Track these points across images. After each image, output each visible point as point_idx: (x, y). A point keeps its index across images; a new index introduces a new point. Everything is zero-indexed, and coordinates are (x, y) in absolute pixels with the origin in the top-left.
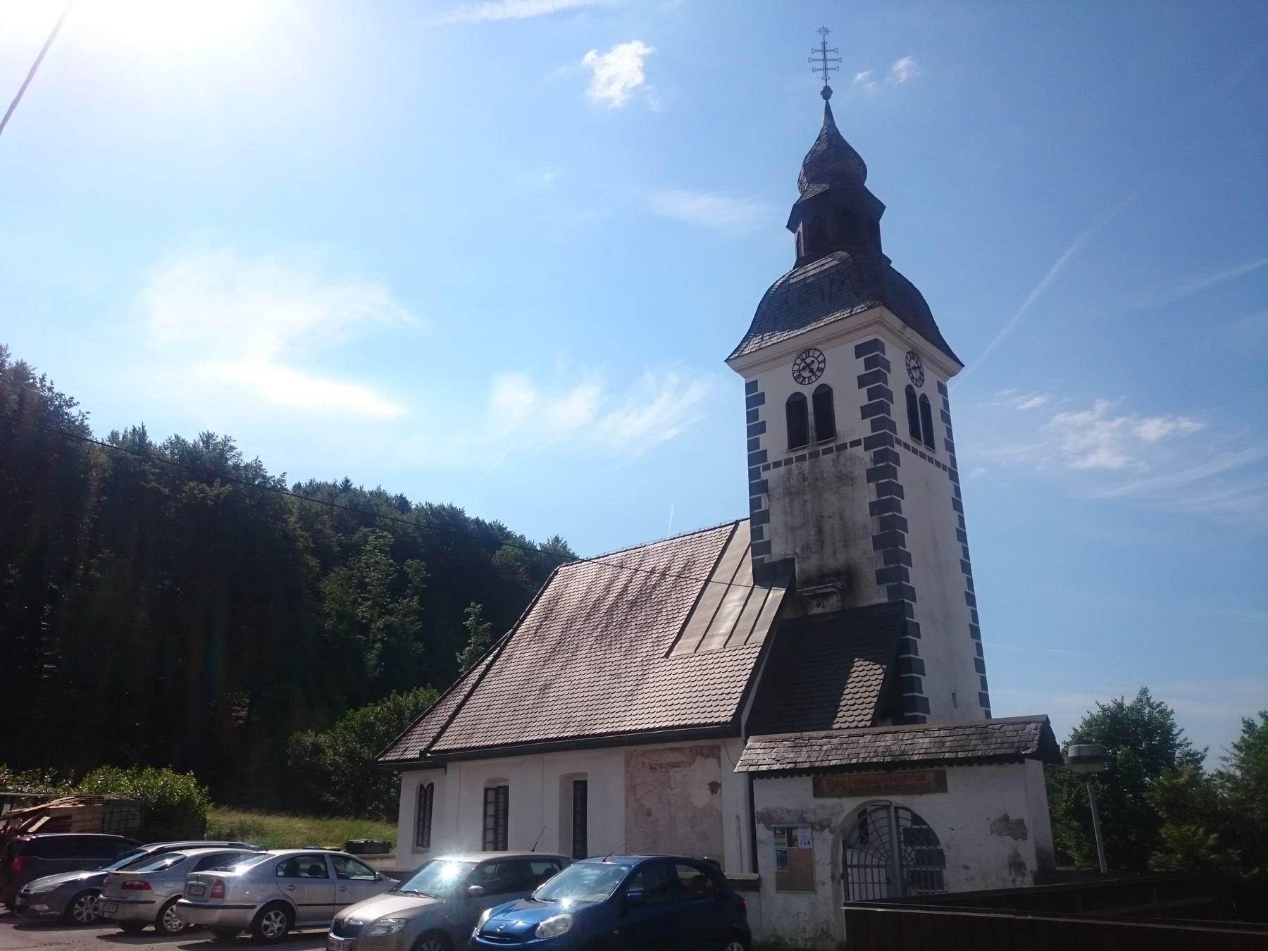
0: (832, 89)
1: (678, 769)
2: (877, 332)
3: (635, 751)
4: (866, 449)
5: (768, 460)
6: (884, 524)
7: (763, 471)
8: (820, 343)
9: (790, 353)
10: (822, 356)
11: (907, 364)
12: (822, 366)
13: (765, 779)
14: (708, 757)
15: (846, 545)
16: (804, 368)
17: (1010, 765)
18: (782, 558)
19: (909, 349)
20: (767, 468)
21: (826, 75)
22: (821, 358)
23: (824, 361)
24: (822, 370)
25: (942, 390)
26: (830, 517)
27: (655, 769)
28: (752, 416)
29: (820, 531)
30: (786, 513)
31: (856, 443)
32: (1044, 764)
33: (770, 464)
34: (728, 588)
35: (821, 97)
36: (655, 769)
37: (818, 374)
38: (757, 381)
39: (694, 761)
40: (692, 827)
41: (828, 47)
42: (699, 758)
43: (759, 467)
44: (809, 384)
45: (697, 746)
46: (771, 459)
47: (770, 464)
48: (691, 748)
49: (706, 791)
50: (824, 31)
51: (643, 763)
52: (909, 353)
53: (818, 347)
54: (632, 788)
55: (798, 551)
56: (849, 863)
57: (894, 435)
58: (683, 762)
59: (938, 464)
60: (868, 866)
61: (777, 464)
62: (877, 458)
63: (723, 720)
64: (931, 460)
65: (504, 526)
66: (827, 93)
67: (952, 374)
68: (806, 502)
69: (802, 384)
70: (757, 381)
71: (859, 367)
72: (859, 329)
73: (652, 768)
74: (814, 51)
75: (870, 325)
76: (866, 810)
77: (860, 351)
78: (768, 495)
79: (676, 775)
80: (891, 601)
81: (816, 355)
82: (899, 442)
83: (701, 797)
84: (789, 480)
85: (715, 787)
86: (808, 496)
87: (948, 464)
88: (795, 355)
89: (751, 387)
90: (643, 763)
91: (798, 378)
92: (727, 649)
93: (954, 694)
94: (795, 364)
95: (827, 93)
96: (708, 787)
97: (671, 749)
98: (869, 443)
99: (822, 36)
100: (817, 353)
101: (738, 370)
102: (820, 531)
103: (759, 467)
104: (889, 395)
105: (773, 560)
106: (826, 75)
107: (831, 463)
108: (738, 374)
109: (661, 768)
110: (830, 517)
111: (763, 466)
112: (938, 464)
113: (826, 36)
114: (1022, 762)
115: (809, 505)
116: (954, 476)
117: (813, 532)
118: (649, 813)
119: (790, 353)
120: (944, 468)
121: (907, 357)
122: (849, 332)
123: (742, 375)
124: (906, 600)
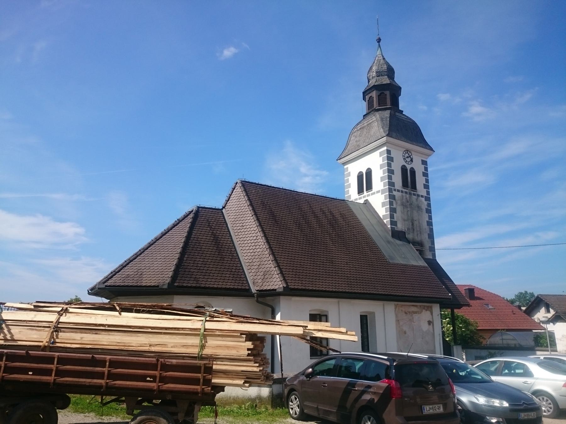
1: (416, 314)
3: (398, 304)
4: (382, 194)
5: (383, 183)
14: (426, 310)
15: (420, 233)
16: (408, 157)
18: (401, 230)
27: (407, 313)
29: (413, 224)
30: (402, 212)
31: (378, 192)
36: (407, 313)
38: (422, 160)
39: (422, 311)
40: (422, 339)
42: (424, 310)
45: (422, 305)
48: (420, 306)
49: (427, 324)
51: (402, 310)
52: (405, 151)
54: (398, 321)
55: (406, 229)
57: (393, 188)
58: (418, 312)
70: (422, 160)
72: (420, 153)
73: (406, 313)
79: (416, 316)
83: (425, 327)
84: (402, 200)
85: (430, 323)
86: (409, 209)
90: (402, 310)
96: (427, 322)
97: (413, 305)
102: (413, 224)
105: (398, 230)
107: (415, 200)
109: (409, 313)
110: (415, 221)
115: (409, 213)
117: (410, 224)
118: (405, 333)
122: (395, 145)
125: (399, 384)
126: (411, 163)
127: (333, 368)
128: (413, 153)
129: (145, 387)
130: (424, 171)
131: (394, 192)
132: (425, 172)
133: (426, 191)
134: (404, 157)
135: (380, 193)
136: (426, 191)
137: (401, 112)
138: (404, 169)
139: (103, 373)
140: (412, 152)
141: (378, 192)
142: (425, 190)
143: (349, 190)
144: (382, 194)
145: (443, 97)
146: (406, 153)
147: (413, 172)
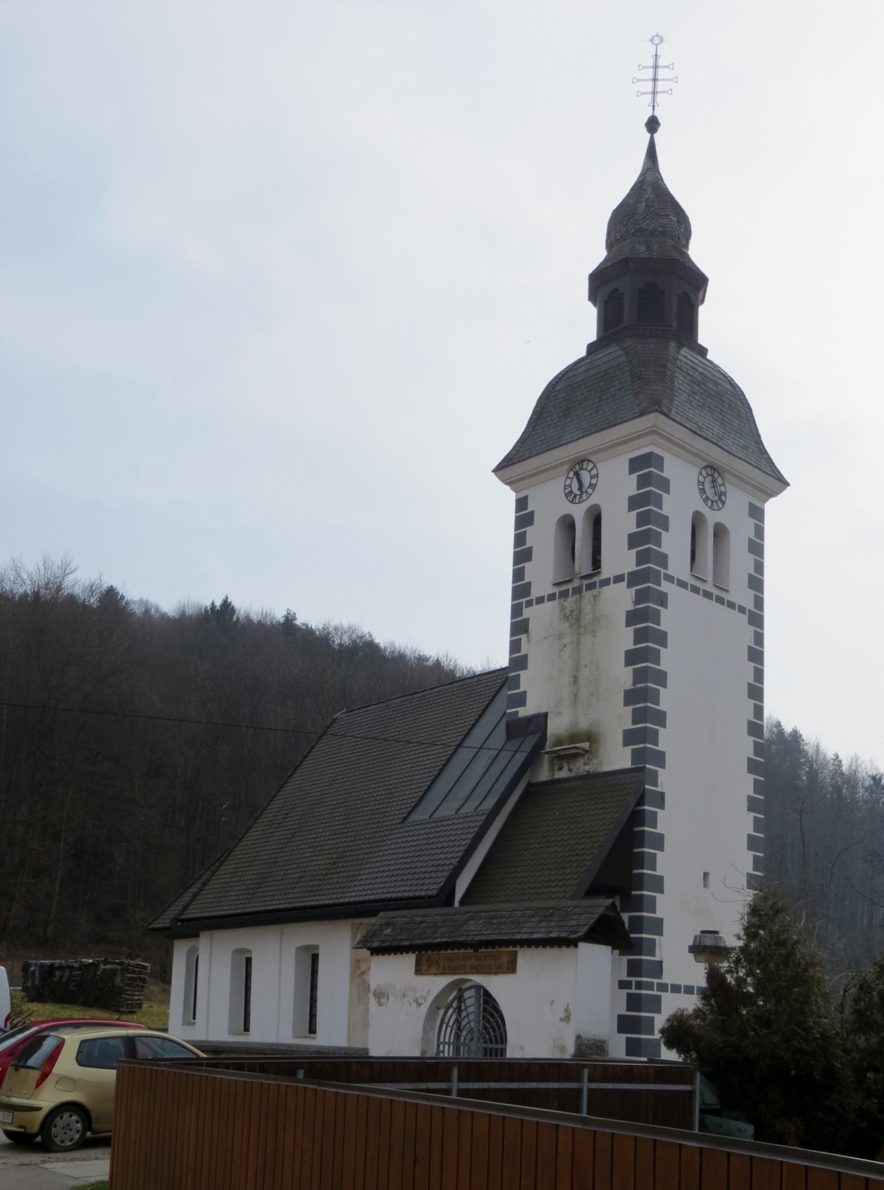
0: (660, 120)
2: (653, 444)
4: (630, 586)
6: (640, 676)
7: (526, 607)
8: (594, 453)
9: (561, 464)
10: (595, 469)
11: (699, 482)
12: (594, 481)
13: (405, 954)
17: (567, 948)
19: (704, 464)
20: (529, 604)
21: (654, 101)
22: (594, 472)
23: (597, 476)
24: (593, 486)
25: (757, 513)
26: (586, 666)
28: (520, 540)
31: (619, 579)
32: (694, 956)
33: (533, 599)
34: (483, 744)
35: (645, 129)
37: (590, 491)
41: (661, 63)
43: (522, 602)
44: (580, 503)
46: (535, 594)
47: (533, 599)
50: (657, 40)
52: (705, 468)
53: (591, 458)
56: (442, 1040)
57: (663, 571)
59: (731, 605)
60: (446, 1043)
61: (540, 600)
62: (641, 596)
63: (430, 893)
64: (720, 600)
65: (414, 649)
66: (653, 125)
67: (774, 493)
68: (565, 646)
69: (572, 502)
71: (630, 485)
74: (641, 67)
75: (646, 434)
76: (461, 988)
77: (635, 464)
78: (528, 636)
80: (633, 766)
81: (589, 468)
82: (669, 578)
87: (750, 605)
88: (566, 467)
89: (521, 504)
91: (571, 496)
92: (457, 817)
93: (706, 875)
94: (567, 478)
95: (653, 125)
98: (634, 579)
99: (654, 47)
100: (591, 466)
101: (509, 482)
103: (522, 602)
104: (664, 522)
106: (654, 101)
108: (508, 487)
111: (526, 601)
112: (731, 605)
113: (659, 47)
114: (576, 946)
116: (756, 620)
119: (561, 464)
120: (742, 610)
121: (700, 474)
123: (513, 489)
124: (648, 766)
125: (430, 952)
126: (721, 506)
127: (172, 944)
128: (727, 476)
129: (29, 1105)
130: (752, 682)
131: (663, 582)
132: (755, 720)
133: (755, 667)
134: (702, 487)
135: (624, 584)
136: (755, 667)
137: (703, 351)
138: (697, 521)
139: (591, 1080)
140: (726, 474)
141: (619, 579)
142: (752, 665)
143: (524, 567)
144: (630, 586)
145: (763, 1030)
146: (708, 475)
147: (720, 532)
